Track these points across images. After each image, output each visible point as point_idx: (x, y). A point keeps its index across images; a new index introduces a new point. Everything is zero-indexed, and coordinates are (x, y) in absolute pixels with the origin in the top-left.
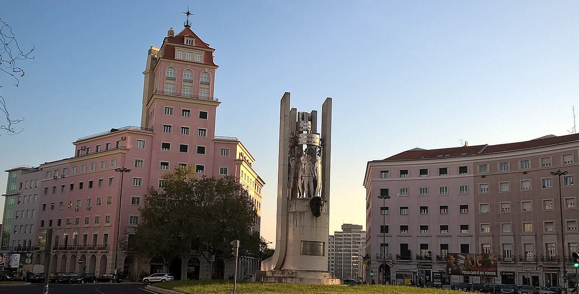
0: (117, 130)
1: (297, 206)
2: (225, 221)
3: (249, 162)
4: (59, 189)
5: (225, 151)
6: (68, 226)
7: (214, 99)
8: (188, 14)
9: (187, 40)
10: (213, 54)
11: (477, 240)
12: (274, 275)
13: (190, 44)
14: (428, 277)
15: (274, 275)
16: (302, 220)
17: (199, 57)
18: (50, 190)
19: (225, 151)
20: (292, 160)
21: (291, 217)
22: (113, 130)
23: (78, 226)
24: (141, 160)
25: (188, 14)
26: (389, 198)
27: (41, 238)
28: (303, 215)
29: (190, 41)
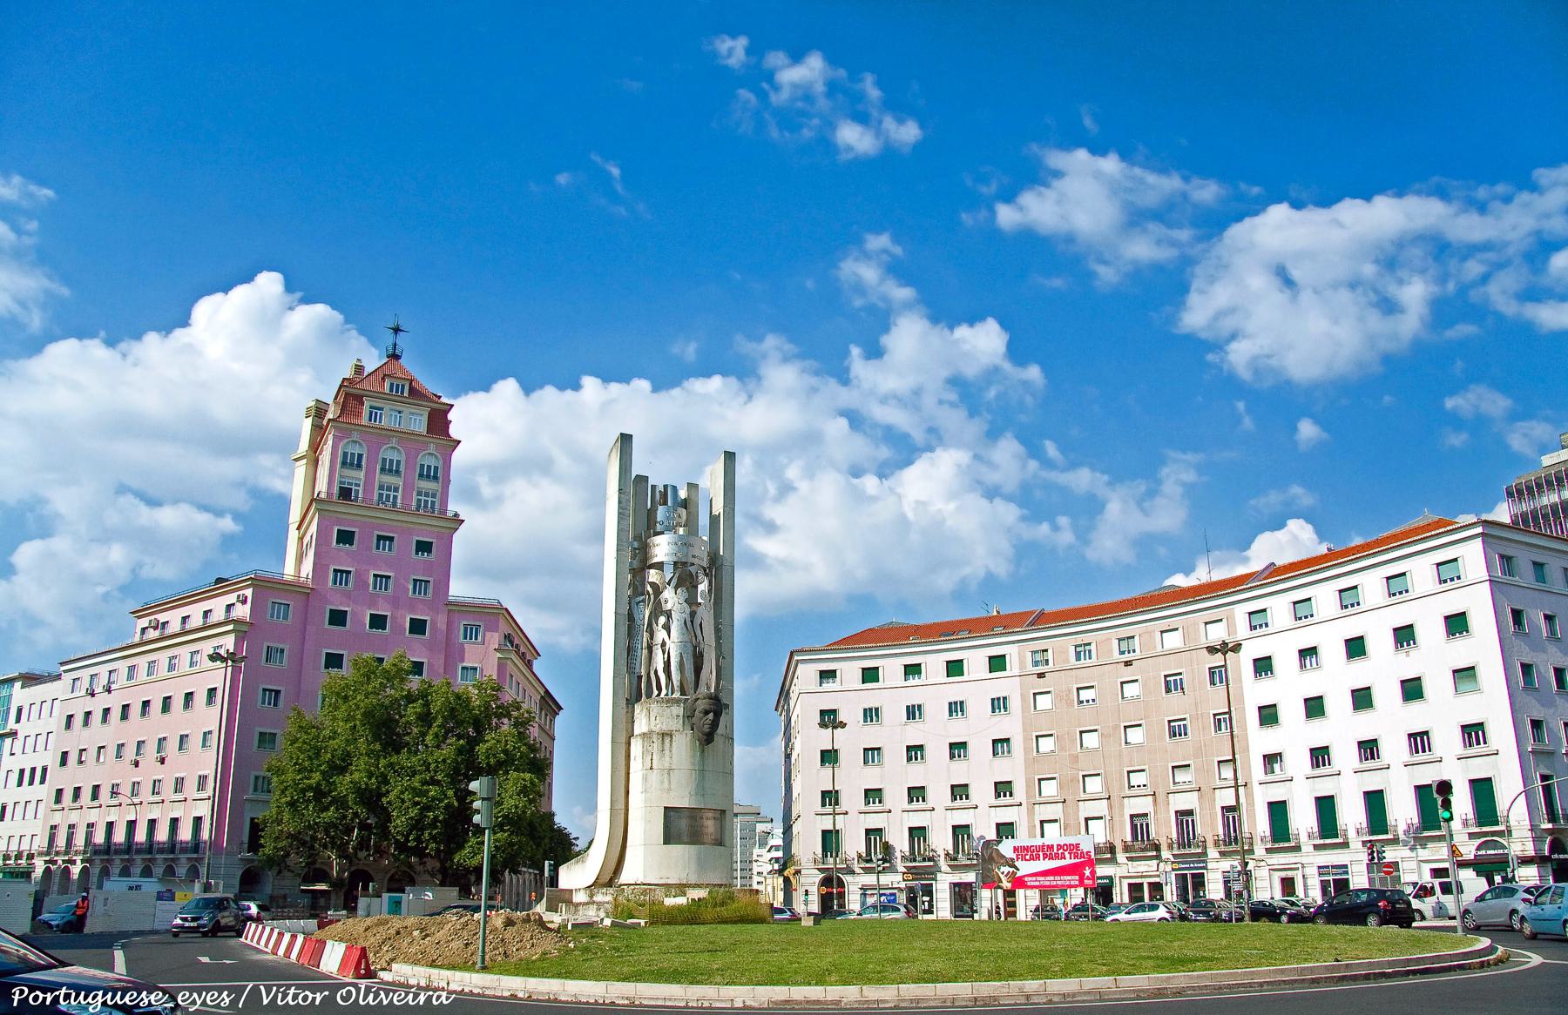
0: (227, 580)
1: (653, 718)
2: (476, 819)
3: (528, 658)
4: (97, 717)
5: (471, 629)
6: (115, 802)
7: (450, 514)
8: (397, 330)
9: (392, 385)
10: (450, 416)
11: (1031, 813)
12: (595, 899)
13: (397, 392)
14: (928, 899)
15: (595, 899)
16: (667, 752)
17: (418, 422)
18: (78, 720)
19: (471, 629)
20: (638, 603)
21: (636, 747)
22: (219, 581)
23: (136, 800)
24: (281, 646)
25: (397, 330)
26: (843, 725)
27: (411, 898)
28: (667, 740)
29: (397, 385)
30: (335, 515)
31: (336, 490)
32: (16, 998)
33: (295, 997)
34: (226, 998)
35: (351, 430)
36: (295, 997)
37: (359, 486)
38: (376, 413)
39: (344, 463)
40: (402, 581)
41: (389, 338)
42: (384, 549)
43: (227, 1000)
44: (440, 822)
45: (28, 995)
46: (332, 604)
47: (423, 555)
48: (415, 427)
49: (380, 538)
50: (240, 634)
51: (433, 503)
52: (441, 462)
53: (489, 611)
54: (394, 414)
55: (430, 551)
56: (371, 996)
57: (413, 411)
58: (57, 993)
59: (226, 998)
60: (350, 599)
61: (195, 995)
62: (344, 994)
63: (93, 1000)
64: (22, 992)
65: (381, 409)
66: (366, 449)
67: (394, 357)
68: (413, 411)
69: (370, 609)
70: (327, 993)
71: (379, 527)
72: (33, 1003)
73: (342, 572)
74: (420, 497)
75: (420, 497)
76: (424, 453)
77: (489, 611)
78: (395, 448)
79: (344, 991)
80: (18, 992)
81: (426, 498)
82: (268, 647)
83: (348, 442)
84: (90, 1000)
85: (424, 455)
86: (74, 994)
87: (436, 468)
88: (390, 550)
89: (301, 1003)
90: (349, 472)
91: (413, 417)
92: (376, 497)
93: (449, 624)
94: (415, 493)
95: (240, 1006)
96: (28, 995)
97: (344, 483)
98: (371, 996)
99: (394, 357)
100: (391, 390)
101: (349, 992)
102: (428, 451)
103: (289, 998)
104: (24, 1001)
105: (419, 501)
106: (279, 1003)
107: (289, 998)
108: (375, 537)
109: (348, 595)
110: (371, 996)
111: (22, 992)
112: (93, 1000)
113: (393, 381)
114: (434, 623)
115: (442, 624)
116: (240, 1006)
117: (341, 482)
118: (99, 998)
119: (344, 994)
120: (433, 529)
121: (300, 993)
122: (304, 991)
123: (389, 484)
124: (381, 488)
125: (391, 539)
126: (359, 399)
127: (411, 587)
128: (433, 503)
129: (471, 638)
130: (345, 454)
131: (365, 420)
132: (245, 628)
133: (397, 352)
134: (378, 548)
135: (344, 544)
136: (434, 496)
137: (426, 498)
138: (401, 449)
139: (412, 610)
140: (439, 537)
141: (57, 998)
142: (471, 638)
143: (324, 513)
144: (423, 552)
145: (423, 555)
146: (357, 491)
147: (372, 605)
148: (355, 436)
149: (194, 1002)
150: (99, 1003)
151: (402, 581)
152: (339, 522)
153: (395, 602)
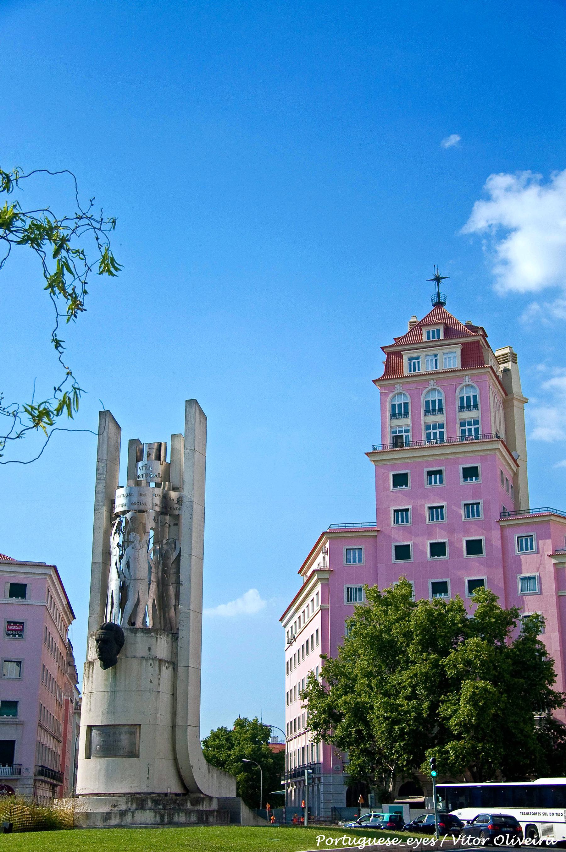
5: (526, 540)
8: (438, 279)
9: (428, 333)
13: (434, 337)
19: (526, 540)
24: (358, 586)
25: (438, 279)
30: (389, 462)
31: (389, 440)
32: (319, 841)
33: (471, 840)
34: (433, 841)
35: (428, 381)
36: (471, 840)
37: (407, 431)
38: (414, 363)
39: (393, 416)
40: (454, 508)
41: (433, 287)
42: (436, 482)
43: (434, 843)
44: (406, 733)
45: (325, 839)
46: (397, 541)
47: (471, 480)
48: (450, 365)
49: (430, 473)
50: (324, 581)
51: (441, 433)
52: (478, 390)
53: (537, 520)
54: (431, 358)
55: (477, 476)
56: (513, 840)
57: (446, 351)
58: (341, 839)
59: (433, 841)
60: (410, 533)
61: (416, 840)
62: (498, 839)
63: (361, 842)
64: (322, 838)
65: (418, 358)
66: (409, 397)
67: (439, 304)
68: (446, 351)
69: (429, 539)
70: (488, 839)
71: (429, 464)
72: (327, 844)
73: (437, 508)
74: (463, 428)
75: (463, 428)
76: (462, 385)
77: (537, 520)
78: (469, 385)
79: (498, 837)
80: (319, 838)
81: (435, 431)
82: (348, 588)
83: (394, 396)
84: (359, 842)
85: (428, 392)
86: (350, 839)
87: (475, 397)
88: (441, 482)
89: (474, 844)
90: (398, 422)
91: (446, 356)
92: (424, 437)
93: (503, 538)
94: (458, 426)
95: (441, 846)
96: (325, 839)
97: (395, 432)
98: (513, 840)
99: (439, 304)
100: (428, 337)
101: (501, 838)
102: (465, 384)
103: (468, 841)
104: (323, 843)
105: (463, 431)
106: (462, 844)
107: (468, 841)
108: (425, 474)
109: (409, 531)
110: (513, 840)
111: (322, 838)
112: (361, 842)
113: (431, 329)
114: (488, 540)
115: (496, 542)
116: (441, 846)
117: (394, 432)
118: (364, 841)
119: (498, 839)
120: (477, 454)
121: (473, 839)
122: (476, 838)
123: (469, 420)
124: (428, 428)
125: (440, 472)
126: (399, 355)
127: (462, 512)
128: (441, 433)
129: (527, 549)
130: (393, 407)
131: (406, 372)
132: (327, 576)
133: (442, 300)
134: (430, 483)
135: (401, 486)
136: (476, 423)
137: (435, 431)
138: (407, 394)
139: (466, 532)
140: (484, 459)
141: (341, 841)
142: (527, 549)
143: (378, 463)
144: (471, 478)
145: (471, 480)
146: (407, 437)
147: (430, 534)
148: (398, 388)
149: (416, 844)
150: (364, 844)
151: (454, 508)
152: (393, 468)
153: (451, 530)
